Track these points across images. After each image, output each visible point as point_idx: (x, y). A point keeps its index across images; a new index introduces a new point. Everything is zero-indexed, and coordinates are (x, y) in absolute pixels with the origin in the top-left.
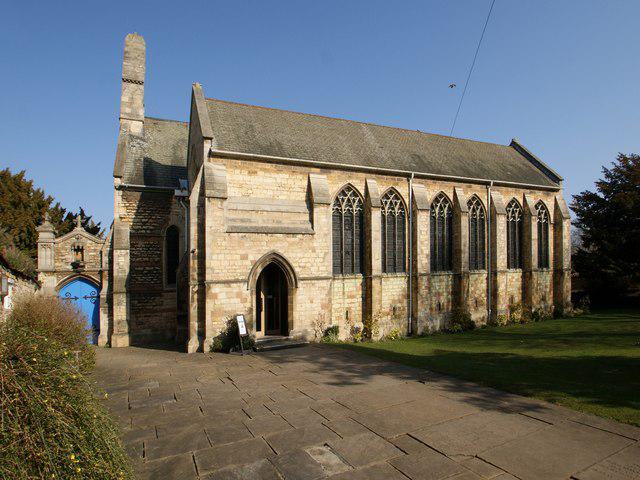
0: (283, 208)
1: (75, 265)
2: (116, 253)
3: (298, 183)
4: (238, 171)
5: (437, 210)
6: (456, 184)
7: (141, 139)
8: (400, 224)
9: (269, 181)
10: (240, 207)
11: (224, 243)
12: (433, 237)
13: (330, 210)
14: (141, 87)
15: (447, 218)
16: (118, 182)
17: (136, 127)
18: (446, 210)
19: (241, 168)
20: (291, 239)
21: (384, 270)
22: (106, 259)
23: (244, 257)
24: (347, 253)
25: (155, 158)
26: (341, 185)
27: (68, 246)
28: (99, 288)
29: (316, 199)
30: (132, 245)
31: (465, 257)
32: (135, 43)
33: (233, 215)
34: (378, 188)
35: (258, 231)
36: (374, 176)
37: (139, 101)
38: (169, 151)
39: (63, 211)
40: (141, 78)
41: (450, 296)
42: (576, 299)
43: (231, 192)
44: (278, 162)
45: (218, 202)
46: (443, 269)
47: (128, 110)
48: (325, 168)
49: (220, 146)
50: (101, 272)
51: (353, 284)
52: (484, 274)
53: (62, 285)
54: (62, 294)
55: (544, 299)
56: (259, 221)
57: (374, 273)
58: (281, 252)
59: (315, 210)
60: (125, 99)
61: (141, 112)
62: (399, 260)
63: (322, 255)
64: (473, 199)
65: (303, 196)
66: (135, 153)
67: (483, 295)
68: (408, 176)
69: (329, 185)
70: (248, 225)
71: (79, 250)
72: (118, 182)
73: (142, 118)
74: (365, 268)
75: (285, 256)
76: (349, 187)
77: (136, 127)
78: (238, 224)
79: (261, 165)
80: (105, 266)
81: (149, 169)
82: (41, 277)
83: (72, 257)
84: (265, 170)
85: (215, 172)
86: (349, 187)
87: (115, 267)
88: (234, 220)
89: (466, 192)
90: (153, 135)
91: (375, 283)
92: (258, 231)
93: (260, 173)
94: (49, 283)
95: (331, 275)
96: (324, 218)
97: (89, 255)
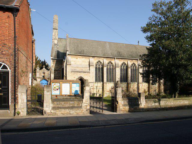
0: (83, 67)
1: (43, 76)
3: (87, 61)
4: (74, 58)
5: (123, 67)
6: (128, 60)
7: (57, 45)
8: (111, 72)
9: (80, 60)
10: (74, 66)
11: (70, 74)
12: (121, 73)
13: (120, 68)
14: (57, 30)
15: (125, 70)
16: (52, 58)
17: (56, 42)
18: (125, 67)
19: (74, 57)
20: (85, 74)
21: (131, 81)
22: (49, 75)
23: (74, 77)
24: (99, 77)
25: (60, 51)
26: (97, 61)
27: (42, 72)
28: (48, 82)
29: (90, 64)
30: (54, 72)
31: (129, 79)
32: (56, 17)
34: (106, 61)
35: (77, 72)
36: (105, 58)
37: (56, 34)
38: (63, 48)
39: (40, 61)
40: (57, 28)
41: (126, 89)
42: (165, 91)
43: (72, 63)
44: (82, 56)
46: (124, 82)
47: (54, 37)
48: (93, 57)
49: (70, 53)
50: (48, 78)
51: (100, 84)
52: (136, 83)
53: (41, 81)
54: (41, 83)
55: (155, 91)
56: (78, 70)
57: (104, 82)
58: (82, 76)
59: (90, 67)
60: (54, 34)
61: (57, 38)
62: (111, 79)
63: (92, 77)
64: (133, 64)
65: (88, 63)
66: (56, 49)
67: (136, 89)
68: (114, 58)
69: (94, 61)
70: (75, 70)
71: (44, 73)
72: (52, 58)
73: (57, 39)
74: (103, 81)
75: (83, 77)
76: (99, 61)
77: (56, 42)
78: (73, 70)
79: (87, 57)
80: (49, 77)
81: (58, 53)
82: (37, 79)
83: (43, 75)
84: (80, 58)
85: (69, 58)
86: (99, 61)
87: (51, 77)
88: (73, 69)
89: (131, 62)
90: (60, 44)
91: (104, 84)
92: (77, 72)
93: (79, 58)
94: (39, 80)
95: (95, 82)
96: (93, 69)
97: (46, 74)
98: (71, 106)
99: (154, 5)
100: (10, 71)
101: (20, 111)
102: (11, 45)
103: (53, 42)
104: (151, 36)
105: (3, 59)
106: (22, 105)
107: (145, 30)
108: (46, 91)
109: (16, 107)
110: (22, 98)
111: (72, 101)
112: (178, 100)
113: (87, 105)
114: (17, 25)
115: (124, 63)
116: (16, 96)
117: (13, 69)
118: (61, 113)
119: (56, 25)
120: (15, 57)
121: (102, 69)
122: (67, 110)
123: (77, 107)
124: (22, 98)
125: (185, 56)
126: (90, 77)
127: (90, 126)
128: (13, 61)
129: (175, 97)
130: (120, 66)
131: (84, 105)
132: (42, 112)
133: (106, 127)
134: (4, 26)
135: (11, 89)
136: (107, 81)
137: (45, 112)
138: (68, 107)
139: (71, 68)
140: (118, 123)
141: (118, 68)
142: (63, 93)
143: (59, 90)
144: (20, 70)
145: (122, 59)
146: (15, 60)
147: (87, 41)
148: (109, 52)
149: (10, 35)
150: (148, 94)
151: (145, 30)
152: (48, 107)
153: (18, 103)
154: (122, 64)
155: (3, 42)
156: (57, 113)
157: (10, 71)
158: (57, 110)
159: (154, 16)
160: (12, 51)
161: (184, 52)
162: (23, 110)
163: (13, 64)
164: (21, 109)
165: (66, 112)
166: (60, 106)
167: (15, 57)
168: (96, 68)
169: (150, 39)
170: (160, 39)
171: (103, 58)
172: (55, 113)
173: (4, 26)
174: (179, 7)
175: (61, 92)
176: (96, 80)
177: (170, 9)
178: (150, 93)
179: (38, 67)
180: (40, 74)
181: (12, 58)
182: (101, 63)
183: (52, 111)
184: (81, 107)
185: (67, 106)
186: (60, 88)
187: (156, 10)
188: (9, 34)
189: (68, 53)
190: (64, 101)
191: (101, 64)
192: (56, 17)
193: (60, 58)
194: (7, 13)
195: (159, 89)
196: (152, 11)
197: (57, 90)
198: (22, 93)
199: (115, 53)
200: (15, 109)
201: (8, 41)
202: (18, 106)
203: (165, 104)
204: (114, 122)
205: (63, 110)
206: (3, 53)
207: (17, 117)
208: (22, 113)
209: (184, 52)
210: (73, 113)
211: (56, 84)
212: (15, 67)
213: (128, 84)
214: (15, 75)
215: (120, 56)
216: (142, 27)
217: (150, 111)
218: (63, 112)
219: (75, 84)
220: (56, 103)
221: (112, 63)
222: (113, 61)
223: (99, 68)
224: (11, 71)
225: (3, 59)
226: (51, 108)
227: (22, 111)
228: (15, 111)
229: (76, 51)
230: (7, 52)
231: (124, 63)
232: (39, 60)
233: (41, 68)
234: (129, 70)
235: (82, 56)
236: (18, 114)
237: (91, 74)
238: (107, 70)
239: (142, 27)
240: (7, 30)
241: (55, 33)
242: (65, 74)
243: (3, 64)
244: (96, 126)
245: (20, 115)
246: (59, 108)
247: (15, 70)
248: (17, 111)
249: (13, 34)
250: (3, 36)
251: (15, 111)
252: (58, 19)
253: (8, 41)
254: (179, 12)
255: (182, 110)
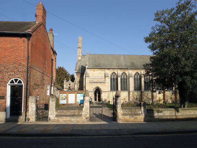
0: (100, 78)
2: (75, 85)
5: (136, 77)
7: (81, 61)
8: (125, 82)
12: (135, 83)
16: (76, 71)
17: (80, 58)
18: (138, 77)
20: (101, 84)
22: (74, 86)
23: (92, 87)
24: (113, 86)
31: (143, 88)
32: (80, 38)
33: (90, 80)
34: (120, 72)
35: (94, 83)
37: (80, 52)
43: (90, 75)
44: (99, 68)
45: (88, 77)
47: (78, 55)
48: (108, 69)
51: (114, 93)
56: (95, 81)
58: (99, 86)
61: (81, 55)
69: (109, 72)
71: (70, 84)
72: (76, 71)
75: (100, 87)
76: (114, 73)
77: (80, 58)
78: (91, 81)
79: (96, 69)
83: (69, 86)
85: (88, 72)
86: (114, 73)
88: (90, 81)
90: (83, 60)
92: (94, 83)
96: (108, 80)
97: (71, 85)
98: (73, 114)
99: (157, 14)
100: (23, 85)
101: (30, 117)
102: (25, 63)
103: (78, 58)
104: (153, 45)
105: (19, 76)
106: (31, 112)
107: (147, 40)
108: (51, 101)
109: (27, 115)
110: (32, 107)
111: (73, 110)
112: (187, 110)
113: (86, 113)
114: (30, 48)
115: (137, 73)
116: (28, 105)
117: (26, 83)
118: (63, 121)
119: (80, 45)
120: (28, 74)
121: (117, 79)
122: (69, 117)
123: (78, 115)
124: (32, 107)
125: (190, 62)
126: (106, 88)
127: (79, 135)
128: (26, 77)
129: (184, 107)
130: (133, 76)
131: (83, 113)
132: (46, 118)
133: (94, 137)
134: (20, 49)
135: (24, 99)
136: (122, 89)
137: (49, 119)
138: (69, 115)
139: (89, 79)
140: (108, 133)
141: (132, 78)
142: (69, 102)
143: (66, 100)
144: (32, 84)
145: (135, 69)
146: (28, 76)
147: (104, 55)
148: (123, 63)
149: (24, 56)
150: (164, 102)
151: (147, 40)
152: (52, 114)
153: (28, 111)
154: (136, 74)
155: (20, 62)
156: (60, 120)
157: (23, 85)
158: (60, 118)
159: (157, 25)
160: (25, 69)
161: (187, 59)
162: (32, 117)
163: (26, 79)
164: (31, 116)
165: (67, 119)
166: (62, 114)
167: (28, 74)
168: (111, 79)
169: (152, 48)
170: (162, 47)
171: (117, 70)
172: (58, 120)
173: (20, 49)
174: (182, 12)
175: (67, 101)
176: (111, 90)
177: (172, 17)
178: (166, 101)
179: (65, 80)
180: (67, 85)
181: (25, 74)
182: (115, 74)
183: (56, 118)
184: (81, 115)
185: (68, 114)
186: (67, 98)
187: (158, 20)
188: (24, 55)
189: (87, 67)
190: (66, 110)
191: (116, 75)
192: (80, 38)
193: (82, 71)
194: (23, 39)
195: (175, 97)
196: (154, 20)
197: (64, 99)
198: (32, 103)
199: (129, 64)
200: (26, 116)
201: (23, 60)
202: (28, 114)
203: (170, 114)
204: (105, 132)
205: (65, 118)
206: (19, 70)
207: (27, 123)
208: (31, 119)
209: (187, 59)
210: (74, 121)
211: (64, 94)
212: (27, 81)
213: (142, 92)
214: (27, 88)
215: (133, 67)
216: (145, 38)
217: (153, 121)
218: (65, 119)
219: (80, 94)
220: (59, 111)
221: (125, 74)
222: (127, 72)
223: (114, 79)
224: (24, 85)
225: (19, 76)
226: (54, 116)
227: (32, 118)
228: (26, 117)
229: (94, 65)
230: (22, 70)
231: (137, 73)
232: (68, 74)
233: (67, 81)
234: (119, 79)
235: (99, 68)
236: (28, 120)
237: (106, 85)
238: (121, 80)
239: (145, 38)
240: (22, 52)
241: (79, 51)
242: (84, 85)
243: (19, 79)
244: (85, 135)
245: (29, 121)
246: (61, 116)
247: (27, 83)
248: (27, 117)
249: (27, 55)
250: (20, 57)
251: (26, 117)
252: (82, 39)
253: (23, 60)
254: (183, 17)
255: (191, 122)
